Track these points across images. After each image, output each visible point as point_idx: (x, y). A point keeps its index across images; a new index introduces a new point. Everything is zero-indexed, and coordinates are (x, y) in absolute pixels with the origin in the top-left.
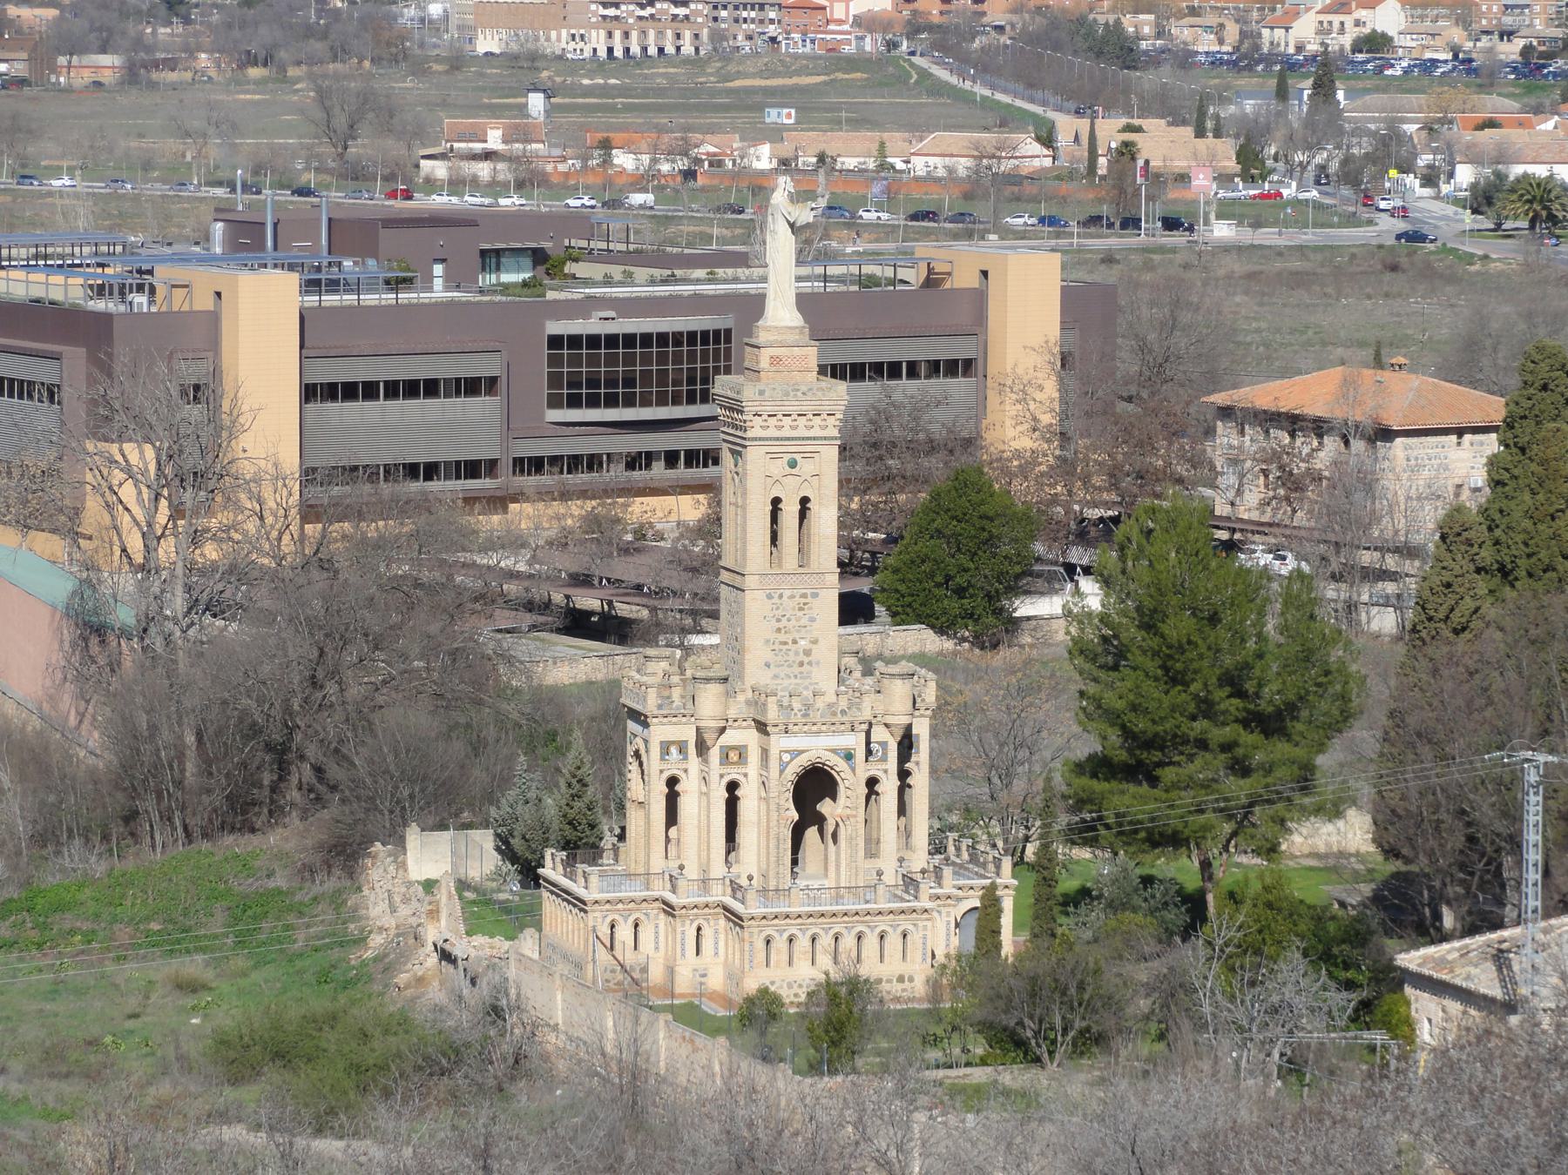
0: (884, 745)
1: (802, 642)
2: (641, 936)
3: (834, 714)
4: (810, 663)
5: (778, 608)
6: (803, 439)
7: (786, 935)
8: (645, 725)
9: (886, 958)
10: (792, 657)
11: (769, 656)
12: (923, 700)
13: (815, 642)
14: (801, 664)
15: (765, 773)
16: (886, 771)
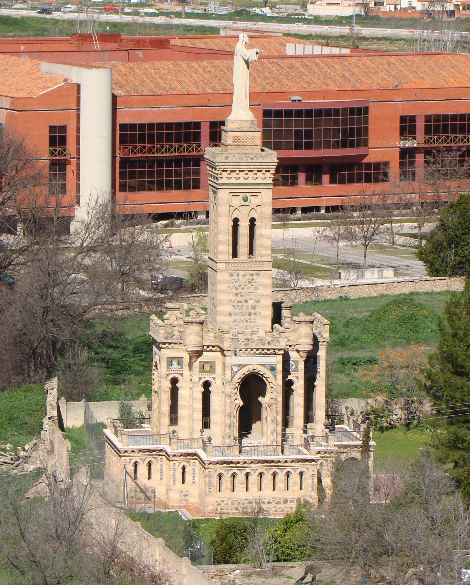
0: (296, 361)
1: (251, 302)
2: (152, 471)
3: (264, 344)
4: (255, 314)
5: (236, 282)
6: (252, 184)
7: (230, 473)
8: (159, 349)
9: (290, 488)
10: (244, 310)
11: (231, 310)
12: (322, 336)
13: (258, 301)
14: (250, 314)
15: (224, 378)
16: (297, 377)
